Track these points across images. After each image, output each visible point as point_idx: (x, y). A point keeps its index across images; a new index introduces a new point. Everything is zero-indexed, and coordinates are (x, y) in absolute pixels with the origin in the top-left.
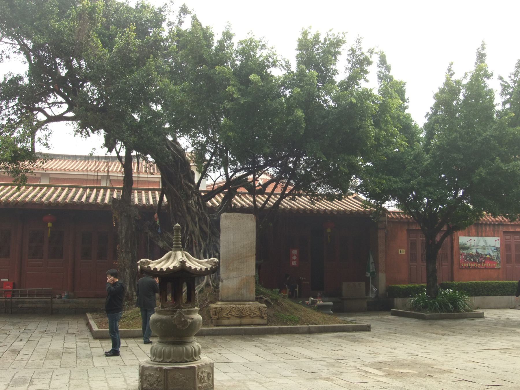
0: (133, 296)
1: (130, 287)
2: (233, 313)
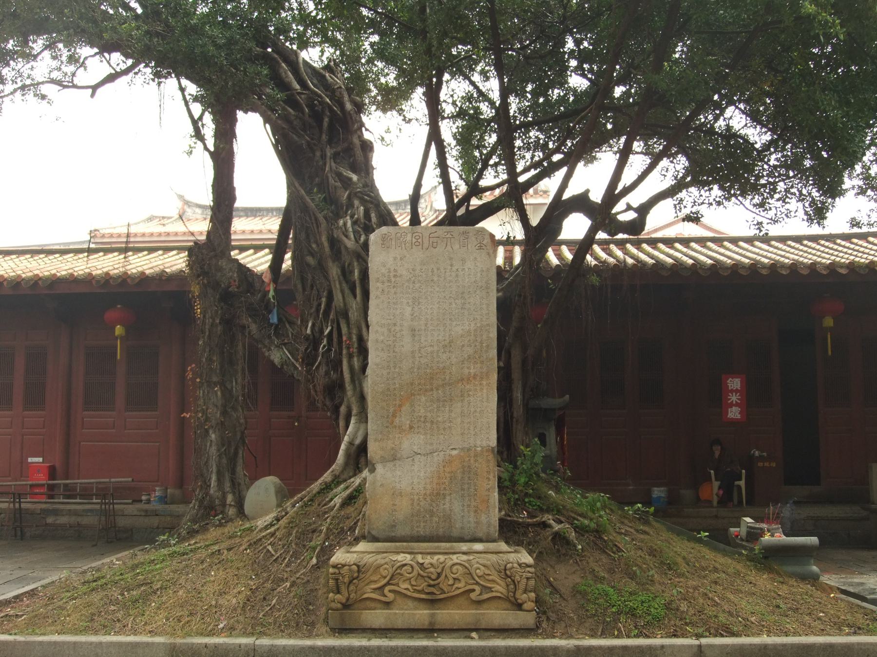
0: (224, 504)
1: (220, 481)
2: (406, 585)
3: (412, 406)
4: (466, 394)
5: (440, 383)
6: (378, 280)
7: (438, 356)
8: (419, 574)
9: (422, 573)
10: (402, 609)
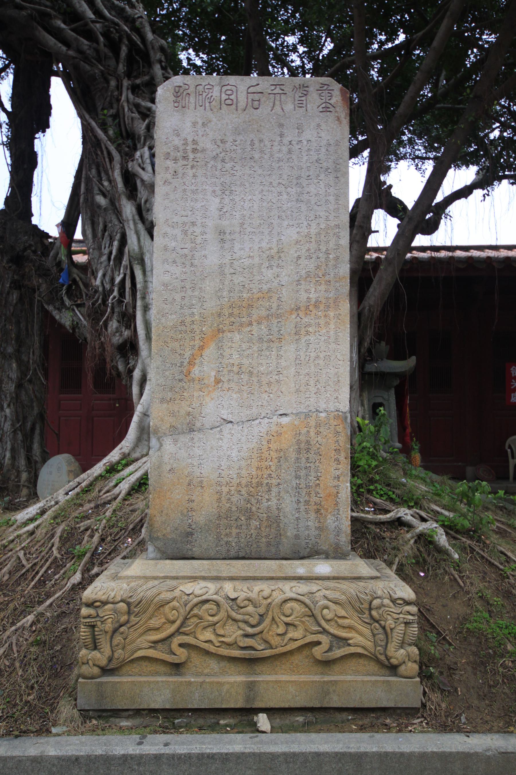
3: (219, 348)
4: (303, 332)
5: (263, 313)
6: (167, 156)
7: (261, 273)
8: (229, 617)
9: (234, 614)
10: (201, 674)
